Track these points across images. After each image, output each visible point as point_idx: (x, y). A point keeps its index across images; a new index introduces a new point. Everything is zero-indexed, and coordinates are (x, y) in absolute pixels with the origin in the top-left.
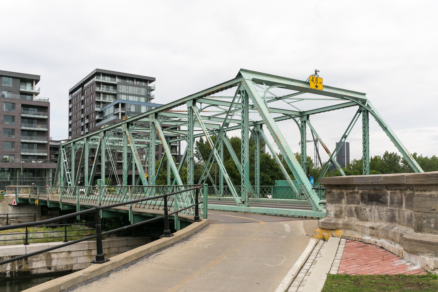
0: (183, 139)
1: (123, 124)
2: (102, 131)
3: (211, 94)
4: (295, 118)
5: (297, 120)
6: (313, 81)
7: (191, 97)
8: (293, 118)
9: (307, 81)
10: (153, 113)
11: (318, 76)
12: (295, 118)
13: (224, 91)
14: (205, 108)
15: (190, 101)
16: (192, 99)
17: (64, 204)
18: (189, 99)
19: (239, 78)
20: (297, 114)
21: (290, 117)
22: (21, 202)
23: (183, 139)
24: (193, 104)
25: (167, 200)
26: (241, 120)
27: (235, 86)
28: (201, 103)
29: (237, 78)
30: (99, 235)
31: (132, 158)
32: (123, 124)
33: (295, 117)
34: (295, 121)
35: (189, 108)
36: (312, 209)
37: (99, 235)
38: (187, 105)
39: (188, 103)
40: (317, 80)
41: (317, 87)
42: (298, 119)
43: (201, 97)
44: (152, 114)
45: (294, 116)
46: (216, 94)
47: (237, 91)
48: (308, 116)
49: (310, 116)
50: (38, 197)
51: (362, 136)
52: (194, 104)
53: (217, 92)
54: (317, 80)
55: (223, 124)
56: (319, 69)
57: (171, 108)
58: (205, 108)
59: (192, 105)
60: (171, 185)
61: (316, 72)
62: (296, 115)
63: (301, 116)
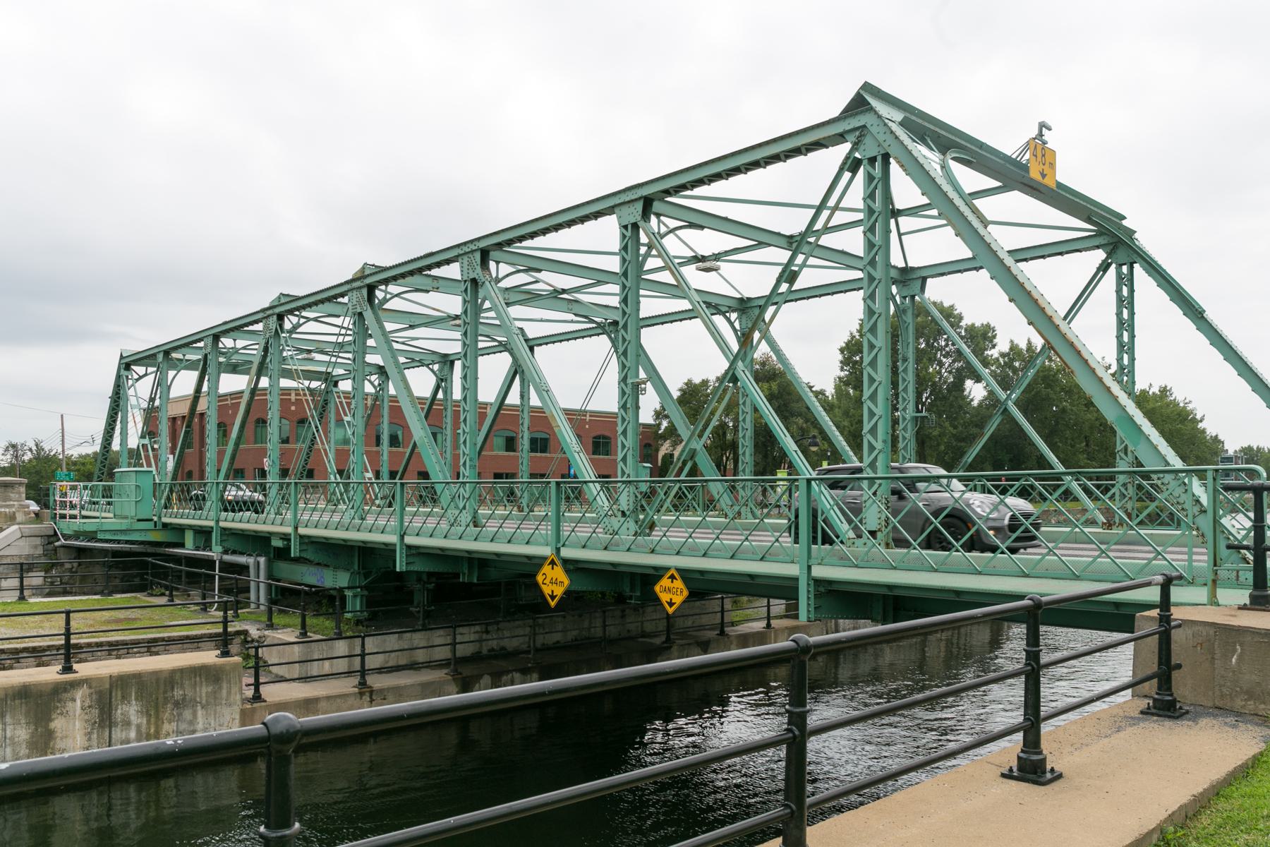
0: (502, 349)
1: (352, 290)
2: (273, 314)
3: (515, 243)
4: (728, 315)
5: (733, 320)
6: (1036, 156)
7: (636, 190)
8: (427, 366)
9: (1014, 156)
10: (473, 251)
11: (1045, 144)
12: (728, 315)
13: (564, 232)
14: (507, 276)
15: (631, 205)
16: (640, 198)
17: (414, 551)
18: (628, 199)
19: (857, 114)
20: (733, 304)
21: (421, 363)
22: (584, 585)
23: (502, 349)
24: (643, 217)
25: (1252, 534)
26: (861, 258)
27: (827, 147)
28: (498, 263)
29: (845, 118)
30: (797, 733)
31: (326, 404)
32: (352, 290)
33: (728, 312)
34: (728, 320)
35: (625, 227)
36: (1039, 546)
37: (797, 733)
38: (619, 218)
39: (625, 210)
40: (1043, 156)
41: (1044, 176)
42: (734, 316)
43: (499, 246)
44: (470, 255)
45: (727, 309)
46: (539, 241)
47: (847, 158)
48: (924, 279)
49: (929, 280)
50: (218, 521)
51: (1116, 339)
52: (646, 214)
53: (439, 267)
54: (1043, 156)
55: (783, 271)
56: (1049, 123)
57: (510, 242)
58: (507, 276)
59: (639, 218)
60: (390, 479)
61: (1042, 126)
62: (729, 307)
63: (901, 282)
